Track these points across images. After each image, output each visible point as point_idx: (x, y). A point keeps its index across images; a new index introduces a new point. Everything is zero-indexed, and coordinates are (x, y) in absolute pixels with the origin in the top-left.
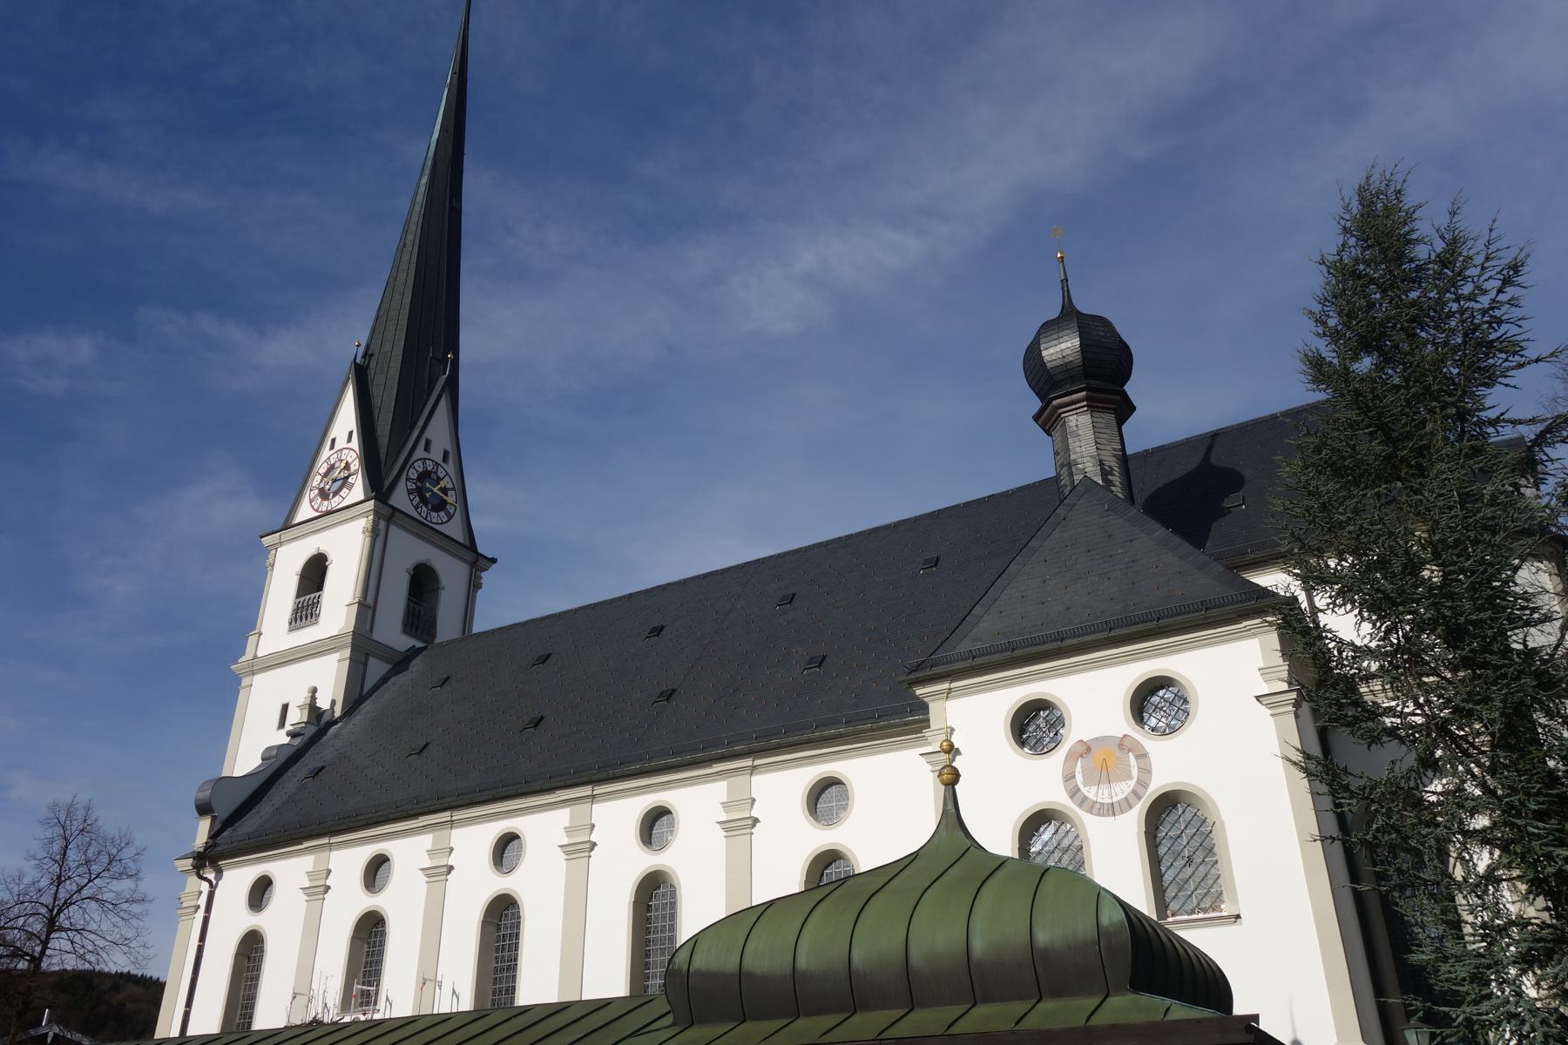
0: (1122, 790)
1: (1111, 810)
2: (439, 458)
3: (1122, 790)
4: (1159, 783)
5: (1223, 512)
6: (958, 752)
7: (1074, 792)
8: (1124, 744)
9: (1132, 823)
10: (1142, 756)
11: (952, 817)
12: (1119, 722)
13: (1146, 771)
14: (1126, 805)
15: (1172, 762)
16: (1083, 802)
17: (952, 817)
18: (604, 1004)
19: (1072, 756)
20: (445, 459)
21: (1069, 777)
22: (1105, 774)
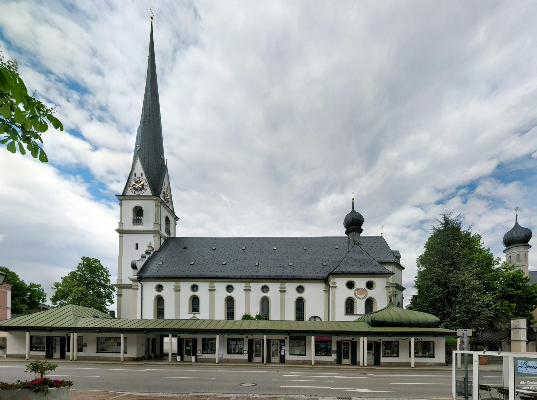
0: (363, 296)
1: (361, 299)
2: (140, 176)
3: (363, 296)
4: (368, 296)
5: (425, 247)
6: (118, 231)
7: (355, 295)
8: (364, 290)
9: (364, 301)
10: (367, 292)
11: (517, 223)
12: (364, 287)
13: (367, 294)
14: (363, 298)
15: (371, 293)
16: (357, 297)
17: (517, 223)
18: (150, 320)
19: (356, 290)
20: (142, 175)
21: (355, 293)
22: (361, 294)
